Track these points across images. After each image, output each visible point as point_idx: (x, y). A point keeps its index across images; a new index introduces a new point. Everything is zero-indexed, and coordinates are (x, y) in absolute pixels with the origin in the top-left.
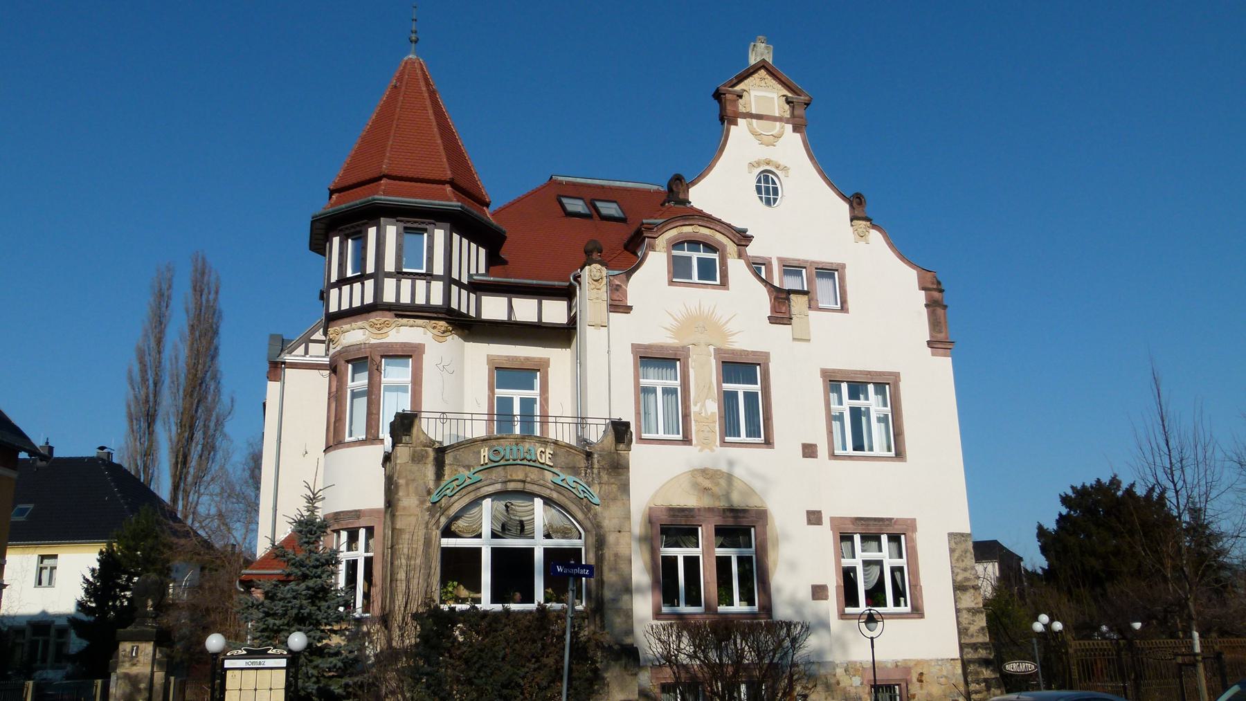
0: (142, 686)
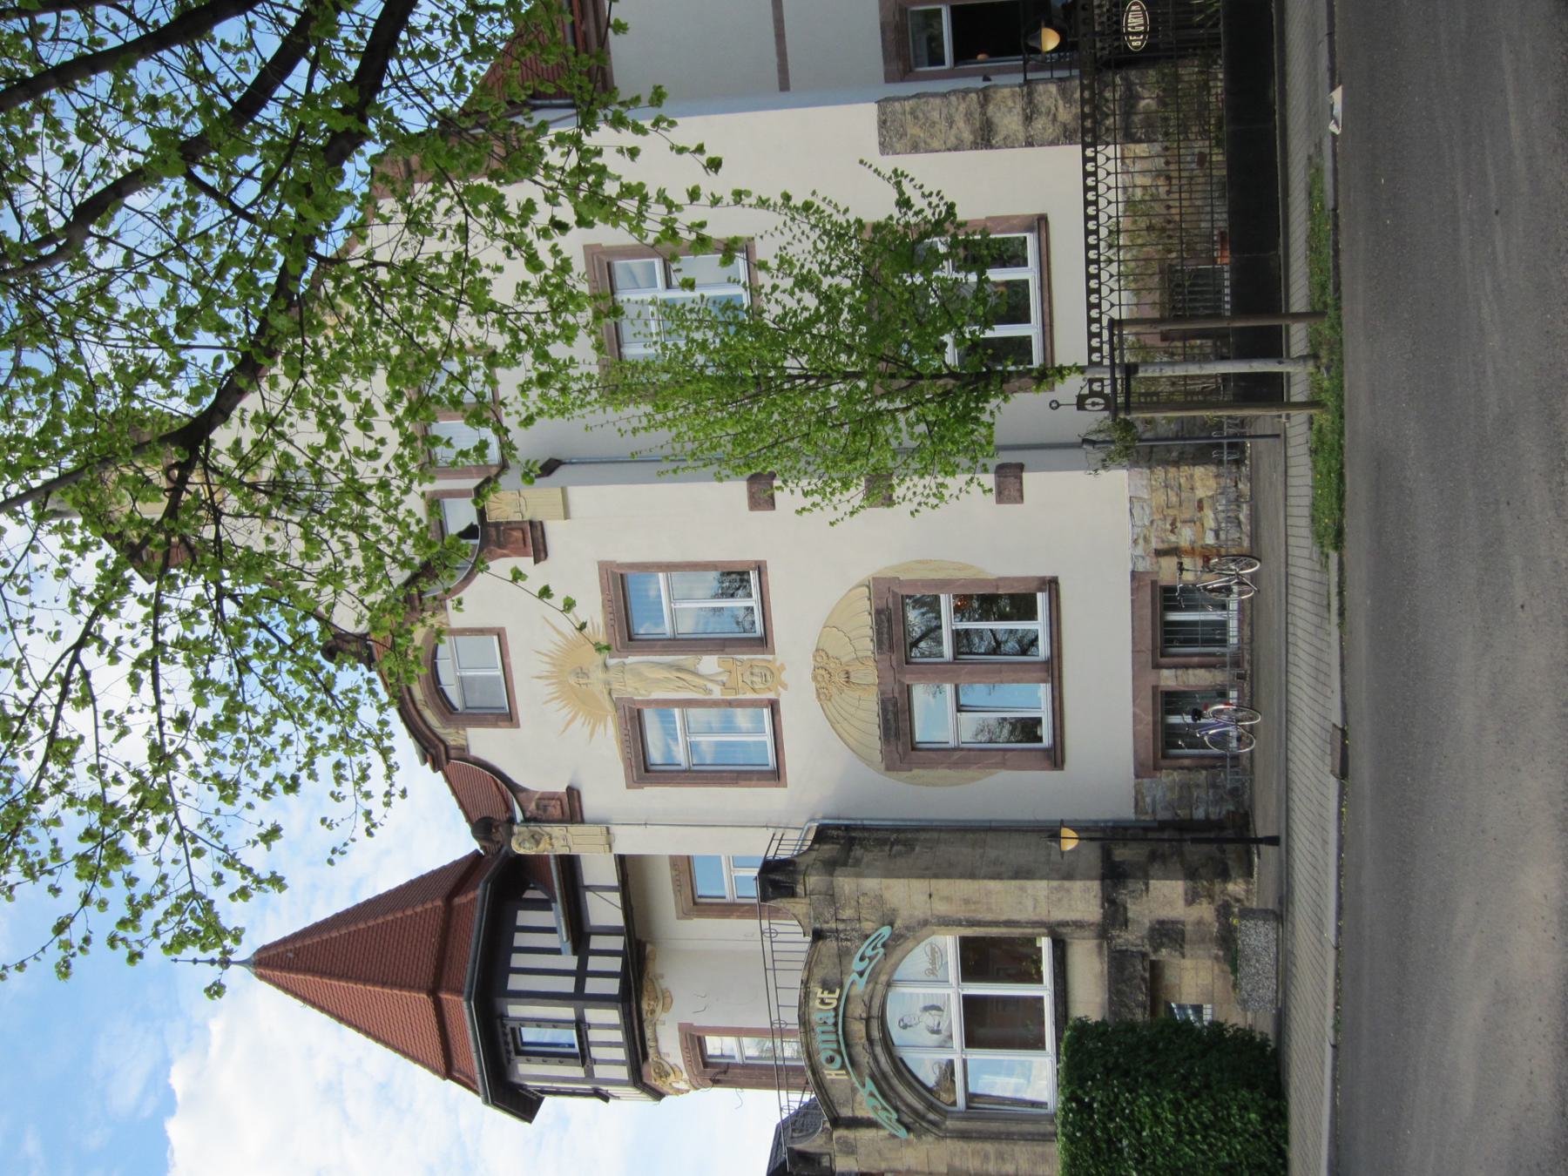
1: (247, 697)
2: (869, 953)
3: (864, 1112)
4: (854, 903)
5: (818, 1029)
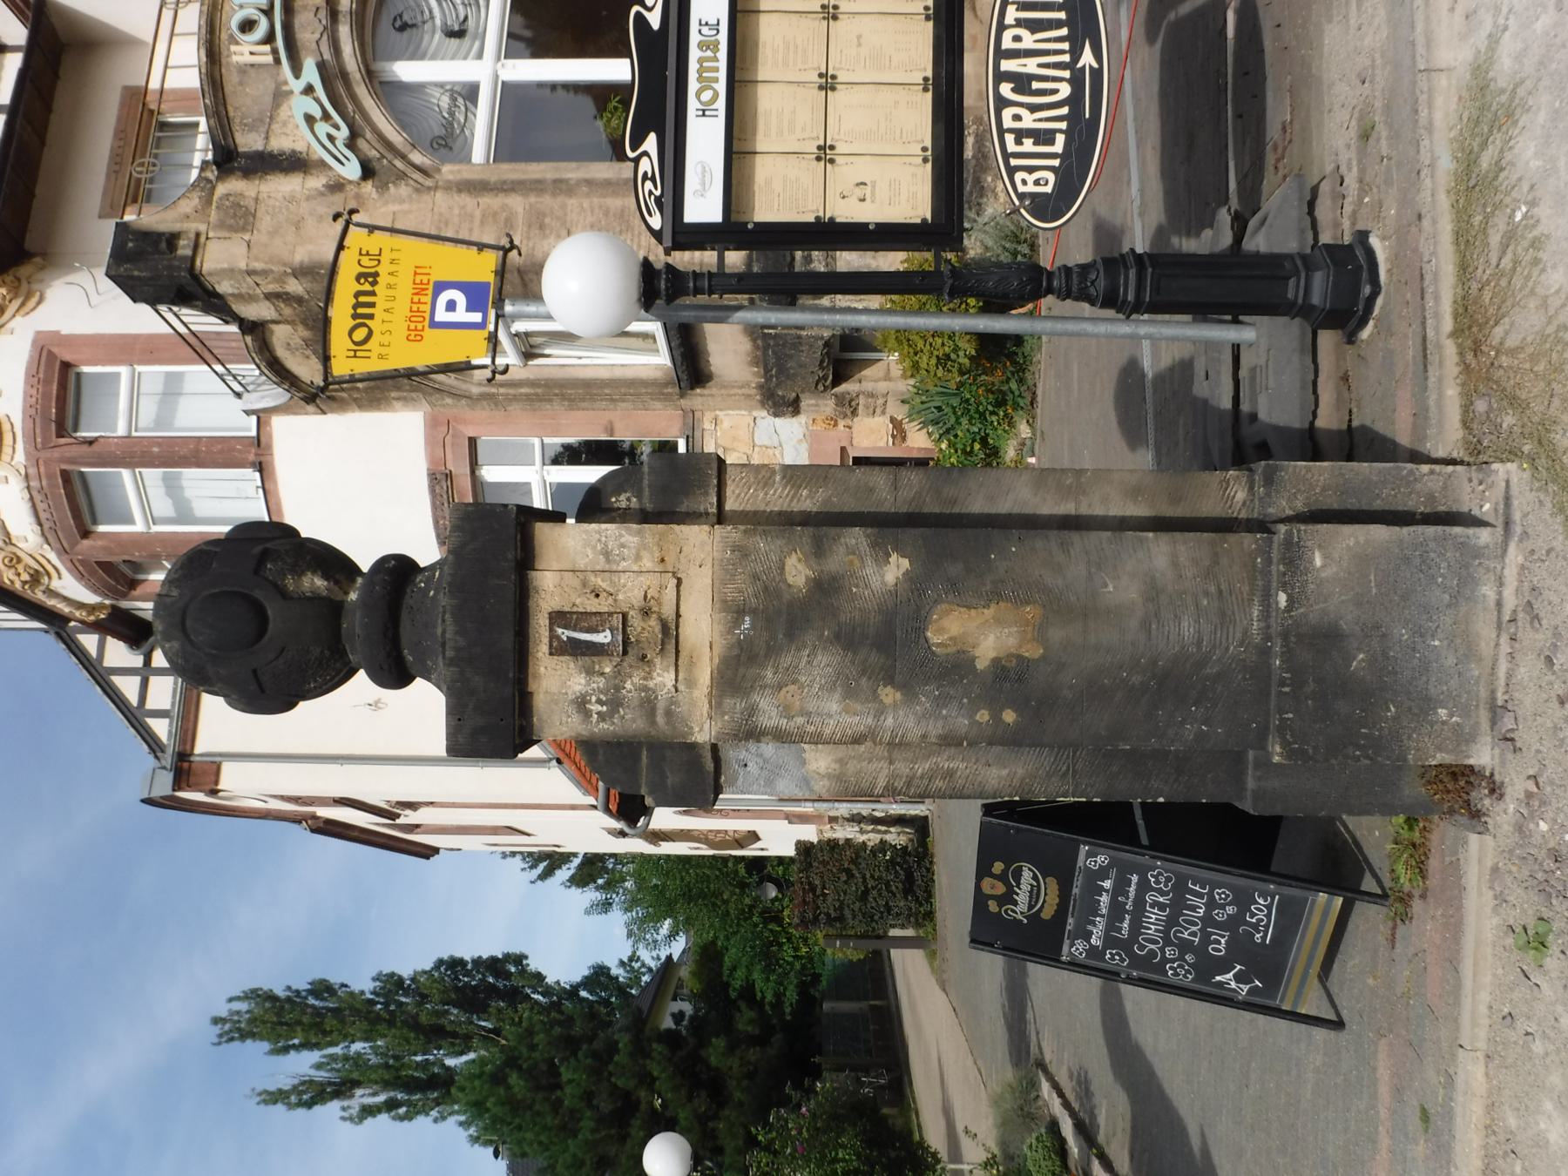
0: (798, 572)
1: (1542, 211)
3: (291, 135)
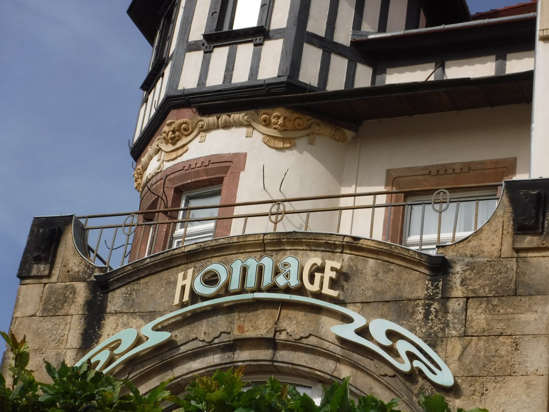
2: (402, 347)
4: (499, 327)
5: (268, 262)
